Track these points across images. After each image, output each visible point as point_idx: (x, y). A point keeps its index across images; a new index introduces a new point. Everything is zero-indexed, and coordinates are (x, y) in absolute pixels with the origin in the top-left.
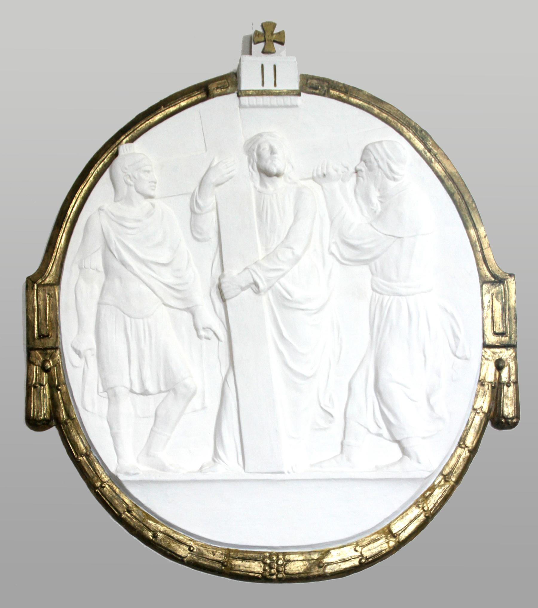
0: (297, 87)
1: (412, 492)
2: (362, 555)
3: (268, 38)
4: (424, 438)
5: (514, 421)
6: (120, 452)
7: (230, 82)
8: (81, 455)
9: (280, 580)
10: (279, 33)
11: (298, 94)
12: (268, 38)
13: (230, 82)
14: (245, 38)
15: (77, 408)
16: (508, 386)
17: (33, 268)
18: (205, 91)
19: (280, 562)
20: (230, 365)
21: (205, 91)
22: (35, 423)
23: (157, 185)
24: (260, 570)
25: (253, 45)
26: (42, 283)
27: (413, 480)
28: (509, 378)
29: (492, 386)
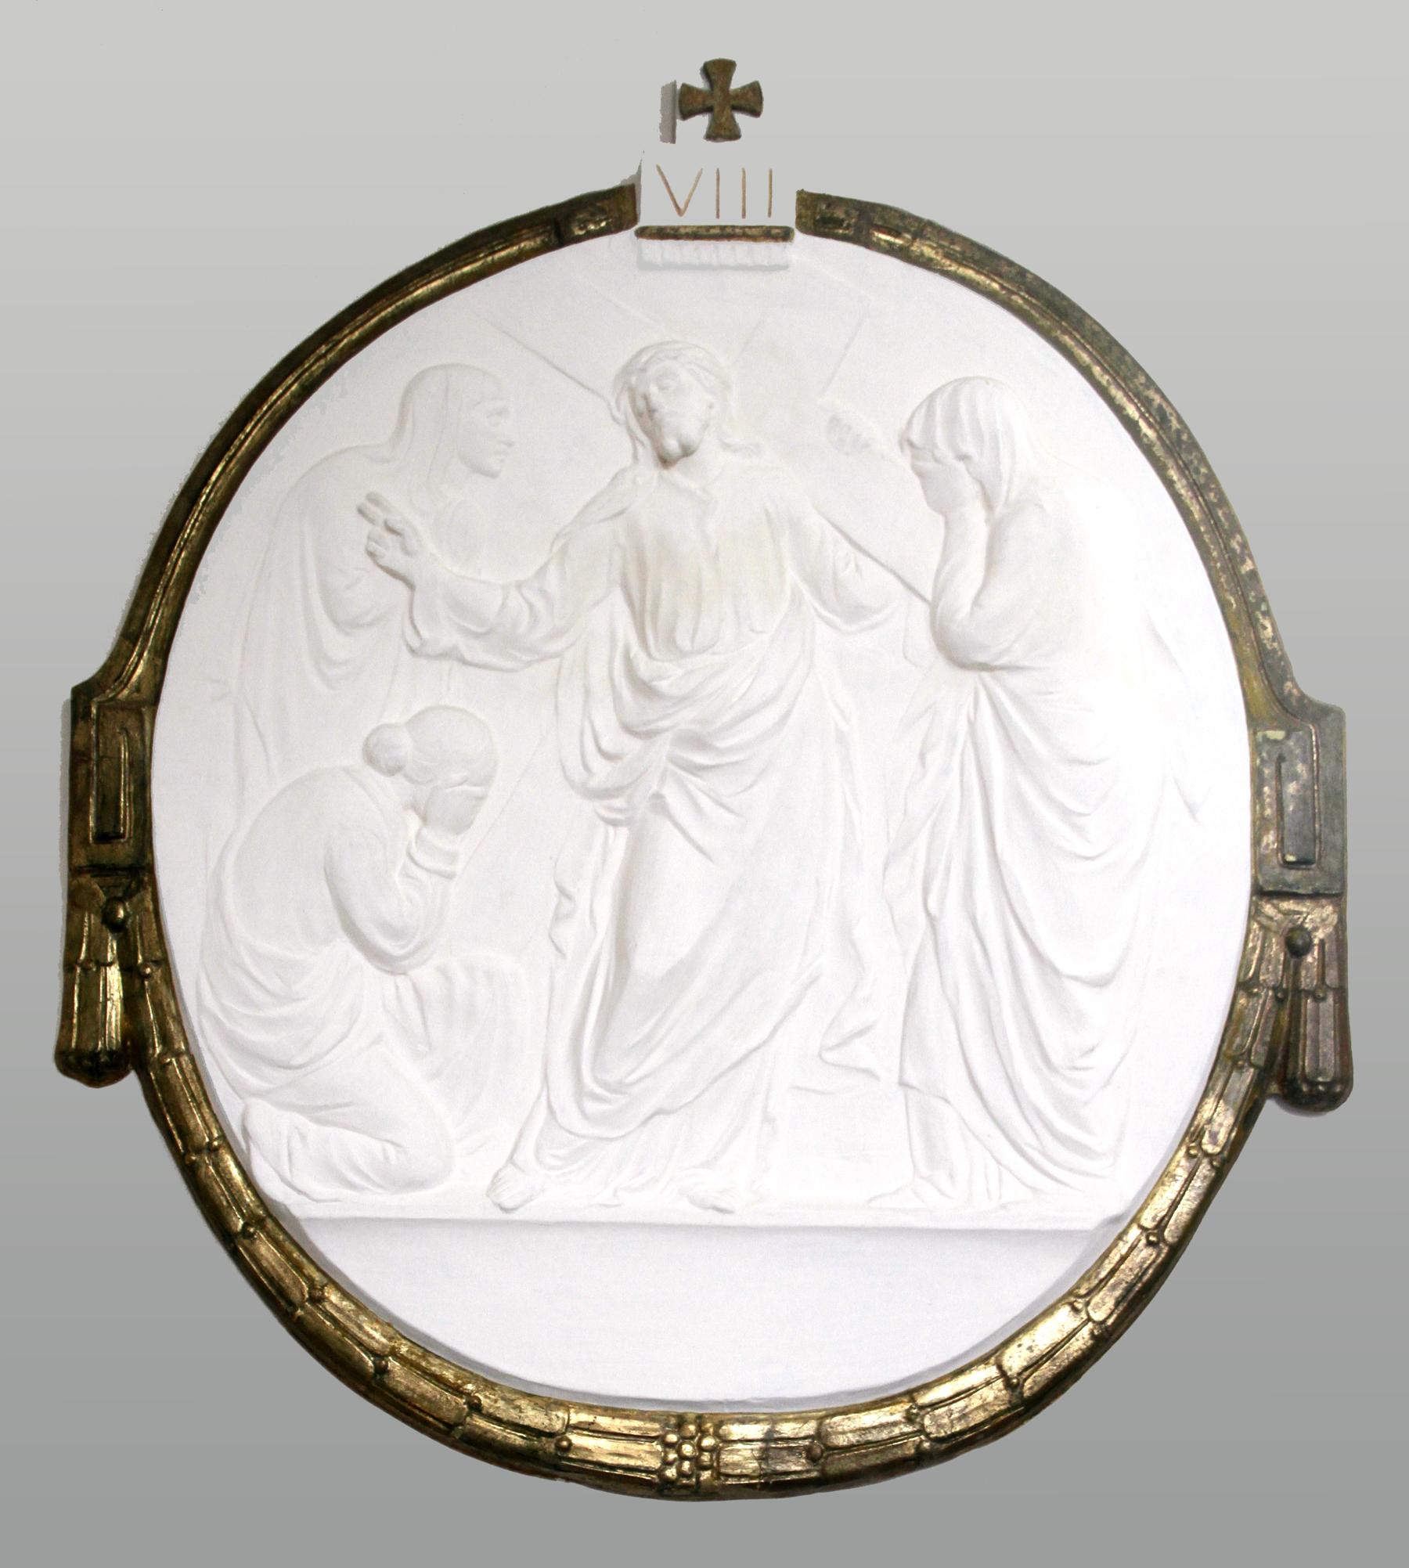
0: (786, 215)
1: (1054, 1270)
2: (922, 1431)
3: (718, 100)
4: (947, 1101)
5: (1338, 1089)
6: (288, 1160)
7: (611, 209)
8: (199, 1151)
9: (699, 1493)
10: (735, 126)
11: (785, 235)
12: (718, 100)
13: (611, 209)
14: (663, 88)
15: (192, 1031)
16: (1317, 1000)
17: (88, 666)
18: (555, 227)
19: (708, 1442)
20: (249, 1164)
21: (555, 227)
22: (85, 1063)
23: (459, 868)
24: (654, 1463)
25: (679, 122)
26: (109, 733)
27: (1059, 1236)
28: (1322, 976)
29: (1276, 997)
